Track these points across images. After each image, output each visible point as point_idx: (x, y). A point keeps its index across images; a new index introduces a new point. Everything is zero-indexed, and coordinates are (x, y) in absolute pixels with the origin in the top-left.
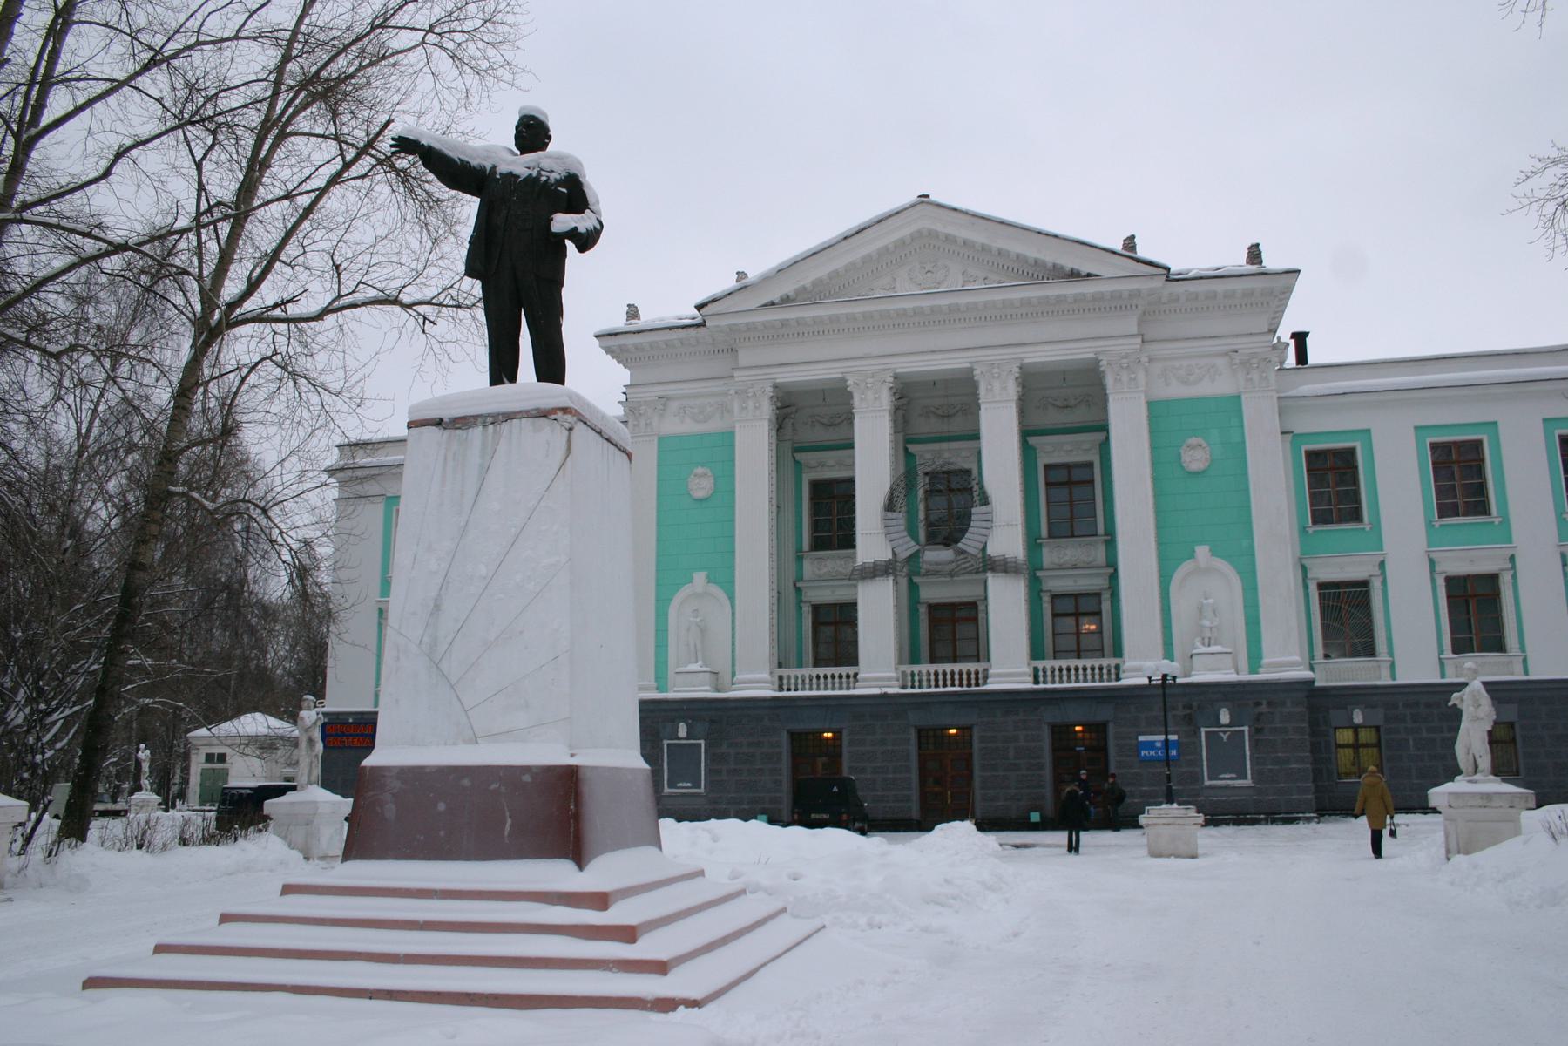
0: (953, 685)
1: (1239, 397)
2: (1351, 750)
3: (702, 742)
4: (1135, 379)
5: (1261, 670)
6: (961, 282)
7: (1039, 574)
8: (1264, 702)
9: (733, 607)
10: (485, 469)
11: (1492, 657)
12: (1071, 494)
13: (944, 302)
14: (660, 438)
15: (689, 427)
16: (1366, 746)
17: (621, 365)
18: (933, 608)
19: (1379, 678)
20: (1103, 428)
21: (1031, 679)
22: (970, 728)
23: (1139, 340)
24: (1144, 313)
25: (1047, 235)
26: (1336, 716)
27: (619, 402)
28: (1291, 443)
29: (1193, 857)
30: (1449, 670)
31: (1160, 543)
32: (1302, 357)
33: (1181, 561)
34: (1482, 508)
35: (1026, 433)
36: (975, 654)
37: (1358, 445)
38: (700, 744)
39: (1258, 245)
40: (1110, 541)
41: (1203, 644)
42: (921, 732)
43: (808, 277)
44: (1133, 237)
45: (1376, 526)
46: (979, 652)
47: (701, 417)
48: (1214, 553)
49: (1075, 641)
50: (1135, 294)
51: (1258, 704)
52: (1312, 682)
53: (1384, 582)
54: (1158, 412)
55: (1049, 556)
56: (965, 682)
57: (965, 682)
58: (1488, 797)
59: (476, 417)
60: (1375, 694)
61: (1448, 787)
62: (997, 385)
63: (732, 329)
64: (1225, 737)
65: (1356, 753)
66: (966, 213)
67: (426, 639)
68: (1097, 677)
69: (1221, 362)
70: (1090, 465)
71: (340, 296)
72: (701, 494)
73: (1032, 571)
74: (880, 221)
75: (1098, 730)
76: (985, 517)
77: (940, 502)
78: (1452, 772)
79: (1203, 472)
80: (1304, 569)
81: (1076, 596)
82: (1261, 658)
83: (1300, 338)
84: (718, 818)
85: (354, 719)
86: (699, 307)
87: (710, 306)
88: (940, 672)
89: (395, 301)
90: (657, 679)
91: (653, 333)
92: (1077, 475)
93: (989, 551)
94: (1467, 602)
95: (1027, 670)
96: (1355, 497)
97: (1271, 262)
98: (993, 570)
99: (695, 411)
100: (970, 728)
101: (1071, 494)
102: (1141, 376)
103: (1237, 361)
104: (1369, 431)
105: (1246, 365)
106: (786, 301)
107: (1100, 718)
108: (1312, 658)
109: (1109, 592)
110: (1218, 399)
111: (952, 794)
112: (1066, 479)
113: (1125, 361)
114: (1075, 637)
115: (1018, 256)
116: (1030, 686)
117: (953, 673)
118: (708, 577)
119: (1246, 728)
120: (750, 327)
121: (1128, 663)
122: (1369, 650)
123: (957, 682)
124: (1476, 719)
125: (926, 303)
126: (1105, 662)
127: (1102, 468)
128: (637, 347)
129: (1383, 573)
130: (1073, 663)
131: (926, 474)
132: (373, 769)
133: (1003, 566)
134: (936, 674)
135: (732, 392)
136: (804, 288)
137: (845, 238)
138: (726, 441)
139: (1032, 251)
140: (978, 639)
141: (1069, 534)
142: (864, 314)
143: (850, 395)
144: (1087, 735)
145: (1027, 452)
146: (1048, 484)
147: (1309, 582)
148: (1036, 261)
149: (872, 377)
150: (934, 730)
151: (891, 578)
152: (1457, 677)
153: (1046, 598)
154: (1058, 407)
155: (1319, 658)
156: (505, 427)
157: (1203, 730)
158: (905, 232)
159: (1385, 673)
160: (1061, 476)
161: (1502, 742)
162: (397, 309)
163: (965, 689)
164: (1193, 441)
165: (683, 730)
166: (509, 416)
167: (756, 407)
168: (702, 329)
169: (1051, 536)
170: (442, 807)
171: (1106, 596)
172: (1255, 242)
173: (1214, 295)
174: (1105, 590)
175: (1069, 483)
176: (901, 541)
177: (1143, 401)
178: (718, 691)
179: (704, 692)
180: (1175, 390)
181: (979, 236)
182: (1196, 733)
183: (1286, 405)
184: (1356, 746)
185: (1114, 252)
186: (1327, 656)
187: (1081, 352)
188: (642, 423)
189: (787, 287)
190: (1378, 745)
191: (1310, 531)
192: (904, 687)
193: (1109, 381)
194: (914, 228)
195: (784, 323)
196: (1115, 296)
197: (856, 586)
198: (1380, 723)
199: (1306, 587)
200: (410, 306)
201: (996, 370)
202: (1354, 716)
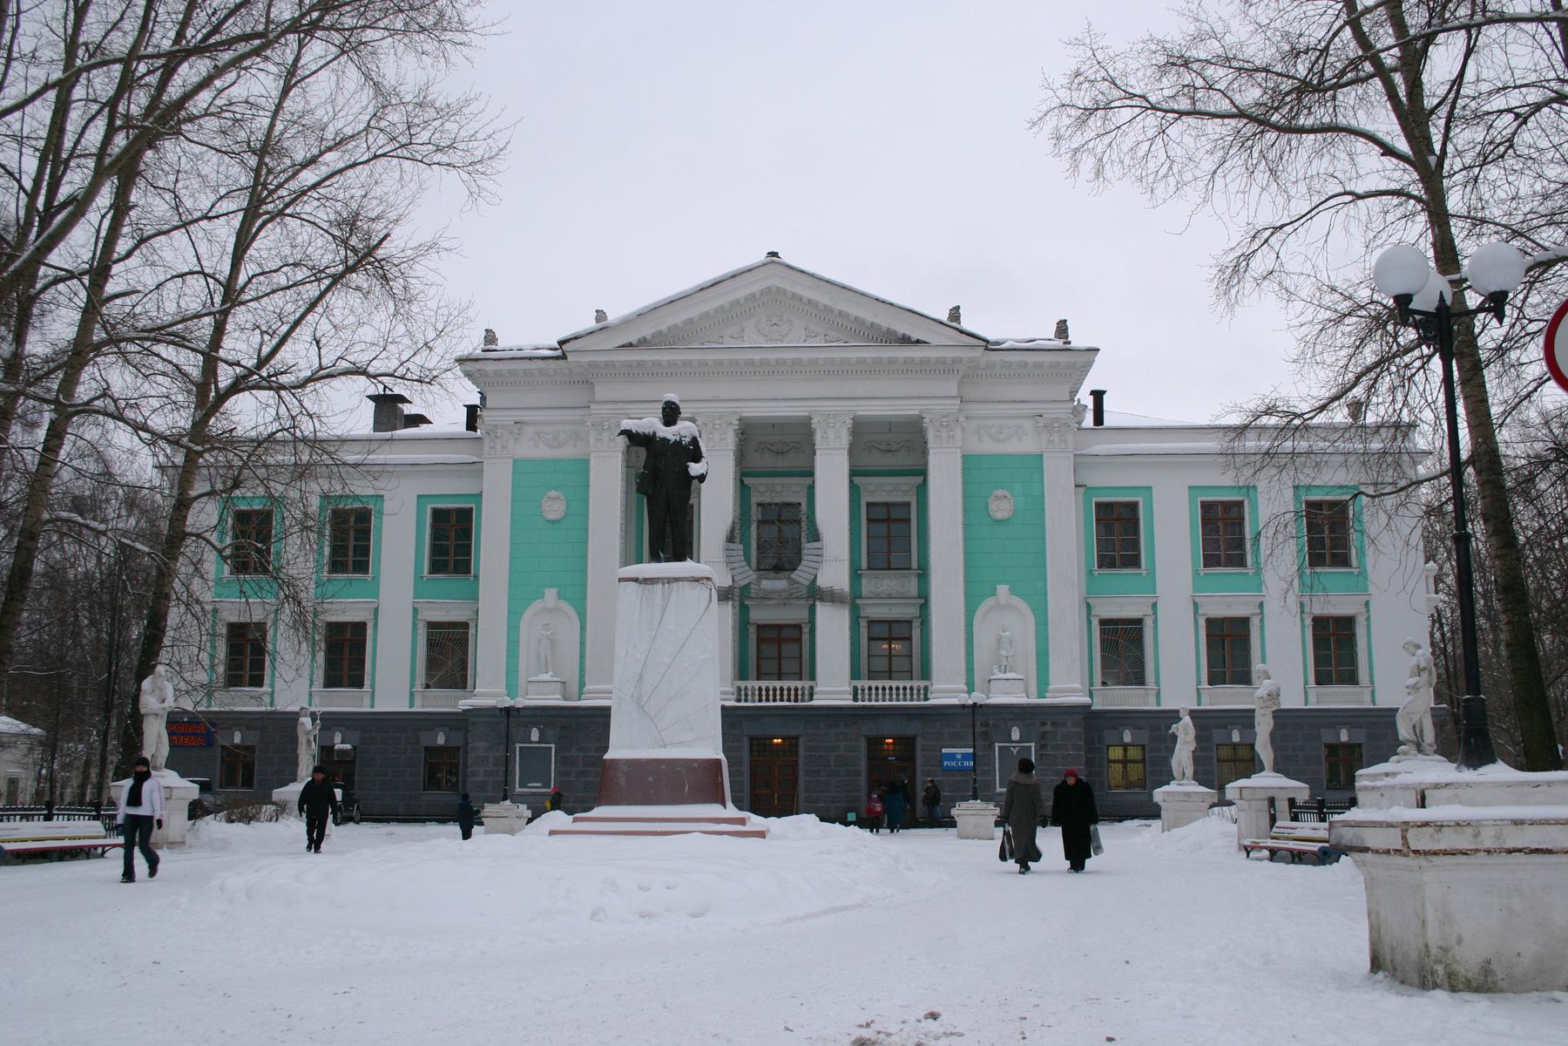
0: (782, 700)
1: (1041, 456)
2: (1120, 765)
3: (553, 746)
4: (953, 436)
5: (1048, 694)
6: (803, 337)
7: (858, 601)
8: (1049, 723)
9: (583, 628)
10: (664, 608)
11: (1239, 688)
12: (889, 529)
13: (789, 356)
14: (514, 461)
15: (544, 452)
16: (1133, 761)
18: (761, 628)
19: (1147, 704)
20: (922, 473)
21: (851, 697)
22: (796, 738)
23: (958, 401)
24: (964, 376)
25: (883, 302)
26: (1109, 736)
27: (1441, 293)
28: (1084, 495)
29: (992, 839)
30: (1205, 699)
31: (967, 581)
32: (1099, 419)
33: (984, 597)
35: (854, 473)
36: (797, 670)
38: (551, 748)
39: (1065, 321)
40: (923, 574)
41: (1000, 671)
42: (751, 739)
43: (664, 323)
44: (958, 308)
45: (1152, 572)
46: (806, 669)
47: (555, 443)
48: (1013, 591)
49: (887, 663)
50: (959, 361)
51: (1044, 724)
52: (1089, 706)
53: (1155, 621)
54: (970, 463)
55: (867, 586)
56: (792, 698)
57: (792, 698)
58: (1188, 794)
59: (658, 579)
60: (1141, 718)
61: (1165, 788)
62: (831, 434)
63: (591, 365)
64: (1015, 751)
65: (1125, 768)
66: (813, 276)
67: (636, 694)
68: (908, 697)
69: (1028, 424)
70: (908, 505)
71: (321, 368)
72: (553, 516)
73: (853, 601)
74: (734, 276)
75: (907, 744)
76: (816, 552)
77: (771, 532)
78: (1167, 777)
79: (1007, 520)
80: (1089, 606)
81: (890, 623)
82: (1048, 684)
83: (1098, 396)
84: (566, 813)
85: (189, 718)
86: (561, 343)
88: (764, 688)
89: (364, 373)
90: (507, 686)
91: (513, 361)
92: (895, 514)
93: (819, 583)
94: (1223, 641)
95: (849, 689)
96: (1135, 544)
97: (1077, 339)
98: (822, 600)
99: (550, 437)
100: (796, 738)
101: (889, 529)
102: (958, 434)
103: (1041, 424)
104: (1150, 488)
105: (1048, 427)
106: (643, 343)
107: (910, 732)
108: (1091, 684)
109: (920, 620)
110: (1023, 457)
111: (779, 796)
112: (885, 517)
113: (945, 419)
114: (887, 659)
115: (856, 318)
116: (850, 703)
117: (782, 689)
118: (558, 594)
119: (1033, 744)
121: (936, 685)
122: (1140, 680)
123: (785, 698)
124: (1185, 742)
125: (772, 356)
126: (915, 684)
127: (918, 508)
128: (497, 373)
129: (1155, 613)
130: (887, 683)
131: (759, 505)
132: (612, 761)
133: (832, 597)
134: (760, 689)
135: (589, 424)
136: (661, 332)
137: (702, 289)
138: (582, 467)
139: (869, 316)
140: (801, 657)
141: (886, 566)
142: (715, 362)
144: (897, 747)
145: (854, 491)
146: (869, 520)
147: (1092, 618)
148: (872, 324)
149: (720, 419)
150: (765, 739)
151: (730, 603)
152: (1211, 704)
153: (863, 624)
154: (882, 451)
155: (1097, 685)
156: (675, 585)
157: (997, 745)
158: (756, 288)
159: (1152, 699)
160: (882, 513)
161: (1245, 761)
162: (363, 378)
163: (793, 704)
164: (1000, 492)
165: (535, 735)
166: (677, 580)
167: (610, 440)
168: (561, 362)
169: (870, 568)
170: (651, 779)
171: (916, 624)
172: (1063, 318)
173: (1025, 365)
174: (916, 618)
175: (888, 520)
176: (740, 570)
177: (959, 455)
178: (566, 700)
179: (555, 701)
180: (987, 446)
181: (822, 298)
182: (991, 747)
183: (1081, 462)
184: (1125, 762)
185: (941, 323)
186: (1104, 684)
187: (908, 409)
188: (498, 446)
189: (646, 331)
190: (1143, 761)
191: (1096, 573)
192: (739, 700)
193: (931, 436)
194: (765, 284)
195: (640, 364)
196: (942, 361)
198: (1146, 742)
199: (1089, 622)
200: (375, 377)
201: (832, 420)
202: (1125, 736)
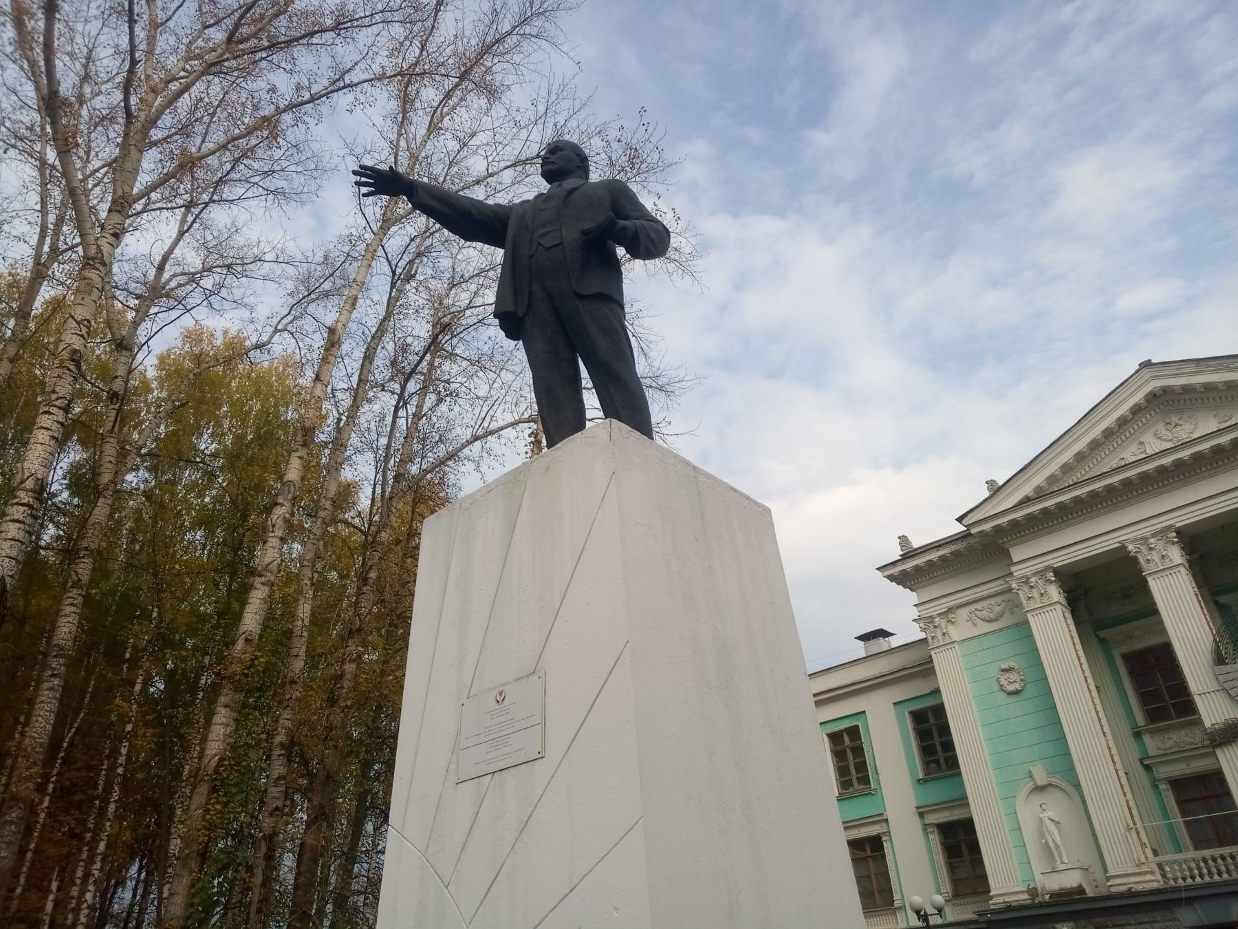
17: (908, 590)
34: (865, 780)
37: (860, 724)
86: (960, 520)
87: (970, 516)
106: (1026, 501)
120: (1014, 524)
143: (1135, 561)
185: (985, 501)
197: (1214, 754)
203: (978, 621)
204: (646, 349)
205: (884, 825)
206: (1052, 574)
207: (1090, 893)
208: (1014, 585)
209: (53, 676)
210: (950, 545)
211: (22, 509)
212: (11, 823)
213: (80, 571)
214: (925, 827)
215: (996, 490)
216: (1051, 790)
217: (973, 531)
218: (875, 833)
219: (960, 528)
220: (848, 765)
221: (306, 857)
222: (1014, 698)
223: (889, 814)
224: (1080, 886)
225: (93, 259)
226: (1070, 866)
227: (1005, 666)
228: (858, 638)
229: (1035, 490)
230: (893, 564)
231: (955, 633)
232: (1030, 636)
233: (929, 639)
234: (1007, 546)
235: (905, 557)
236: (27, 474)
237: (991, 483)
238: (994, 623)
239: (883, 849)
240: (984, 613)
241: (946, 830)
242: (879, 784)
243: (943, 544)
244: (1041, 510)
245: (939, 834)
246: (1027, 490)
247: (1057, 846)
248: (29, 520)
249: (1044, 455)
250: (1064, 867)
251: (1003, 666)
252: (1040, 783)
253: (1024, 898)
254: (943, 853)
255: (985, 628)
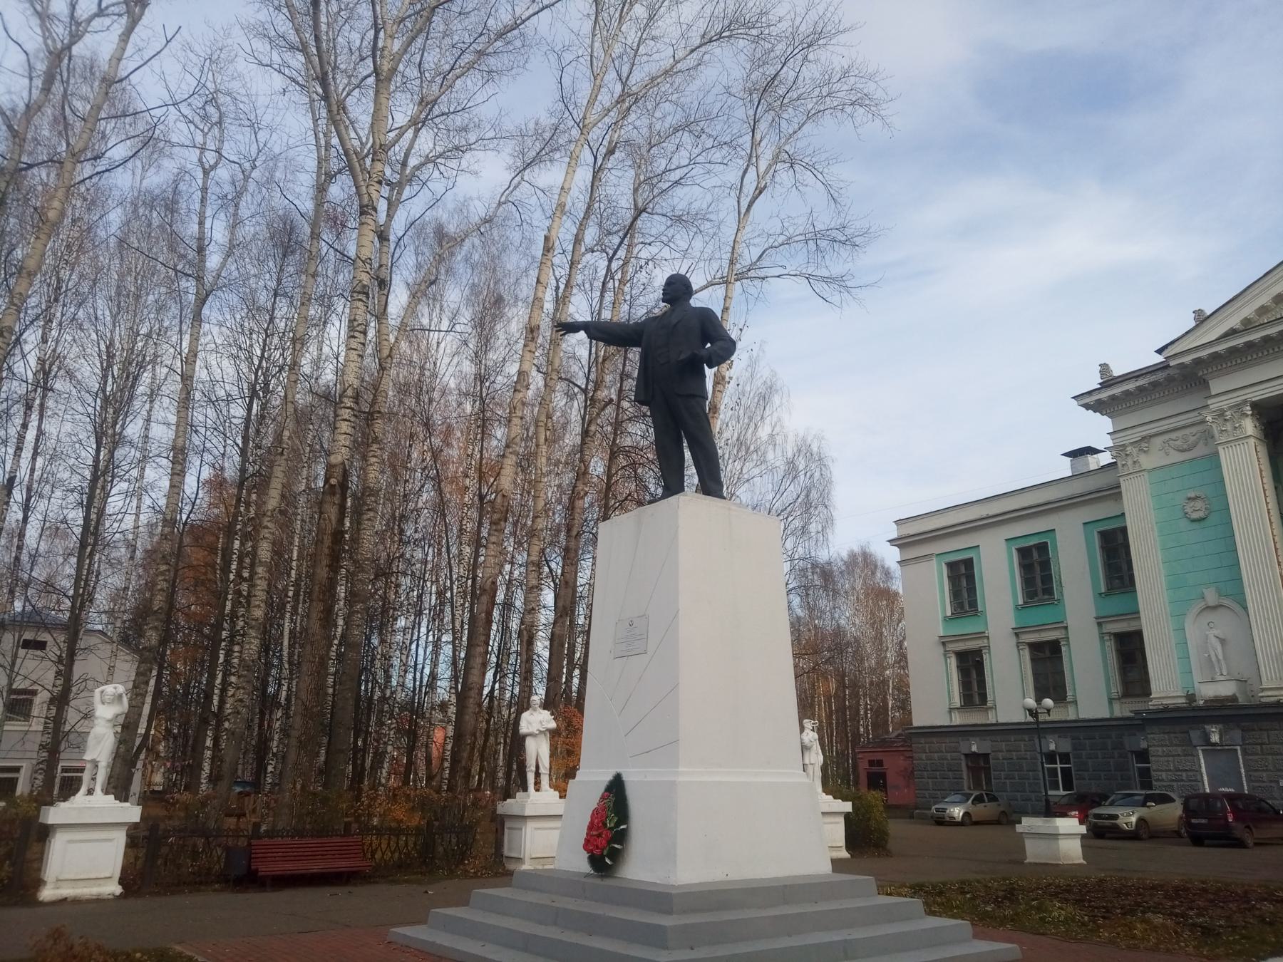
34: (1048, 591)
86: (1160, 351)
87: (1170, 348)
106: (1232, 333)
120: (1215, 357)
203: (1172, 451)
204: (835, 195)
205: (986, 641)
206: (1249, 408)
207: (1242, 701)
208: (1209, 418)
209: (369, 510)
210: (1149, 376)
211: (348, 411)
212: (358, 612)
213: (376, 430)
214: (1102, 635)
215: (1202, 319)
216: (1221, 610)
217: (1172, 364)
218: (1054, 638)
219: (1159, 359)
220: (1034, 578)
221: (555, 643)
222: (1195, 525)
223: (1070, 622)
224: (1234, 695)
225: (367, 206)
226: (1228, 678)
227: (1193, 495)
228: (1067, 455)
229: (1242, 322)
230: (1090, 393)
231: (1147, 462)
232: (1219, 466)
233: (1119, 465)
234: (1205, 377)
235: (1105, 385)
236: (347, 385)
237: (1198, 313)
238: (1186, 453)
239: (1060, 651)
240: (1178, 443)
241: (962, 656)
242: (1062, 595)
243: (1142, 375)
244: (1245, 343)
245: (1116, 642)
246: (1234, 321)
247: (1218, 660)
248: (353, 419)
249: (1257, 285)
250: (1222, 678)
251: (1189, 495)
252: (1211, 604)
253: (1181, 701)
254: (1118, 658)
255: (1176, 457)
